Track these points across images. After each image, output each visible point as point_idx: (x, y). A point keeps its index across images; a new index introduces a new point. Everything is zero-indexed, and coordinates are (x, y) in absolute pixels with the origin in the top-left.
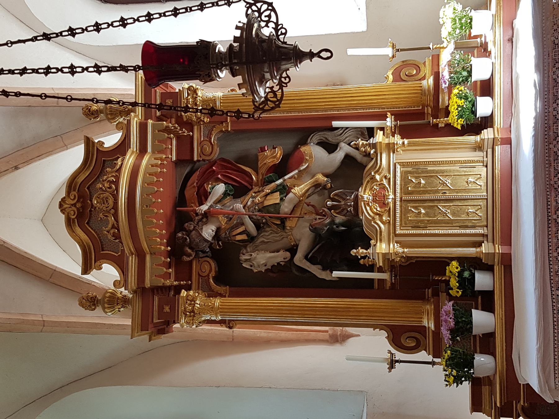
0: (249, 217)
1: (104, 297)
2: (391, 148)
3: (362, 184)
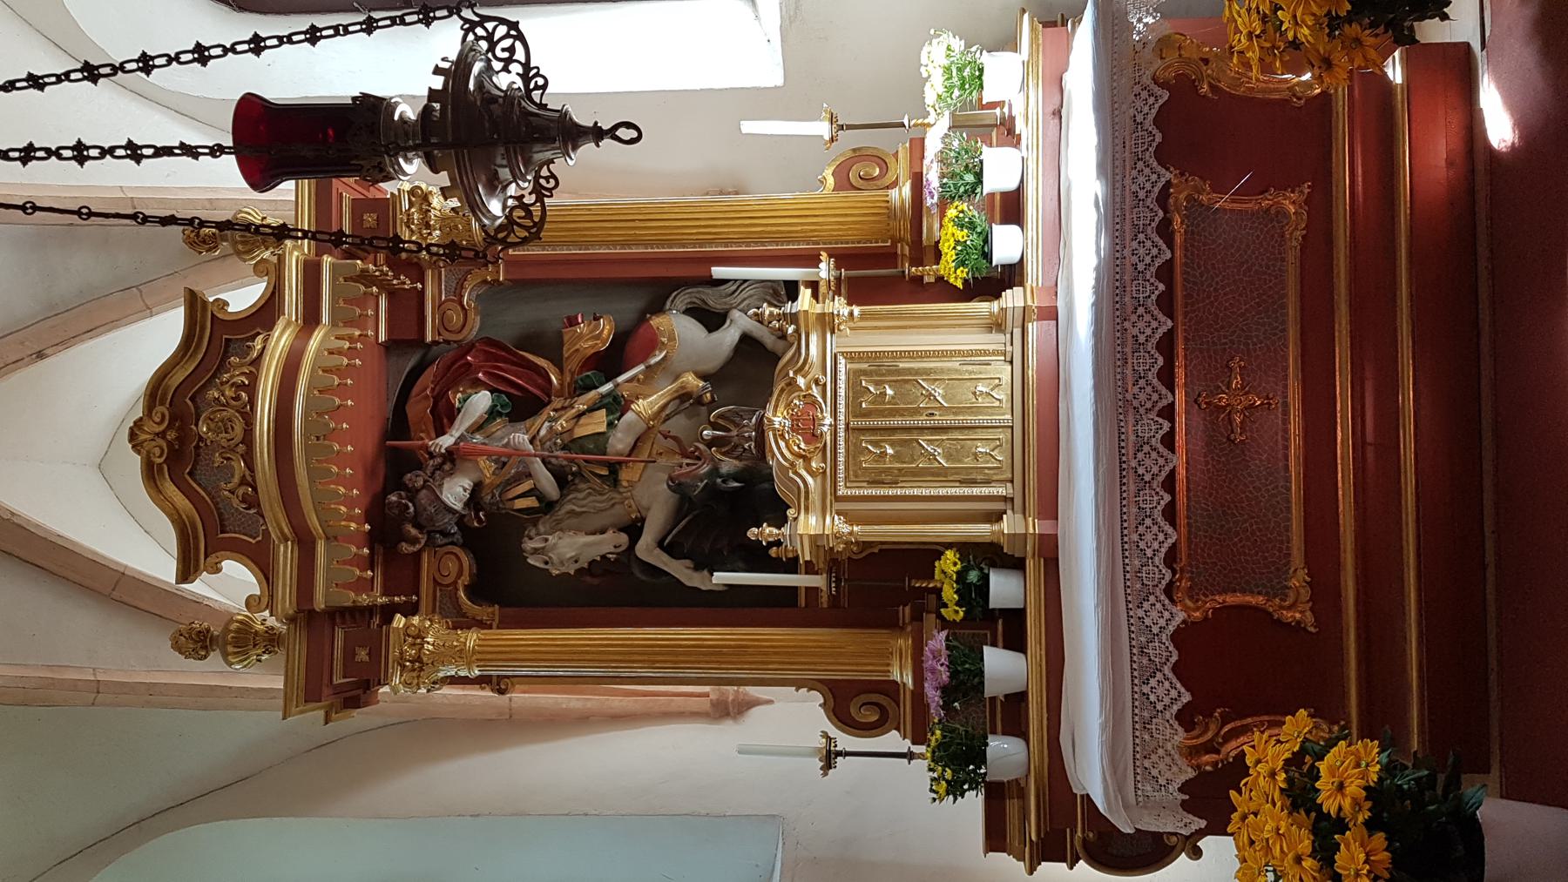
0: (543, 461)
1: (226, 630)
2: (827, 323)
3: (771, 394)
